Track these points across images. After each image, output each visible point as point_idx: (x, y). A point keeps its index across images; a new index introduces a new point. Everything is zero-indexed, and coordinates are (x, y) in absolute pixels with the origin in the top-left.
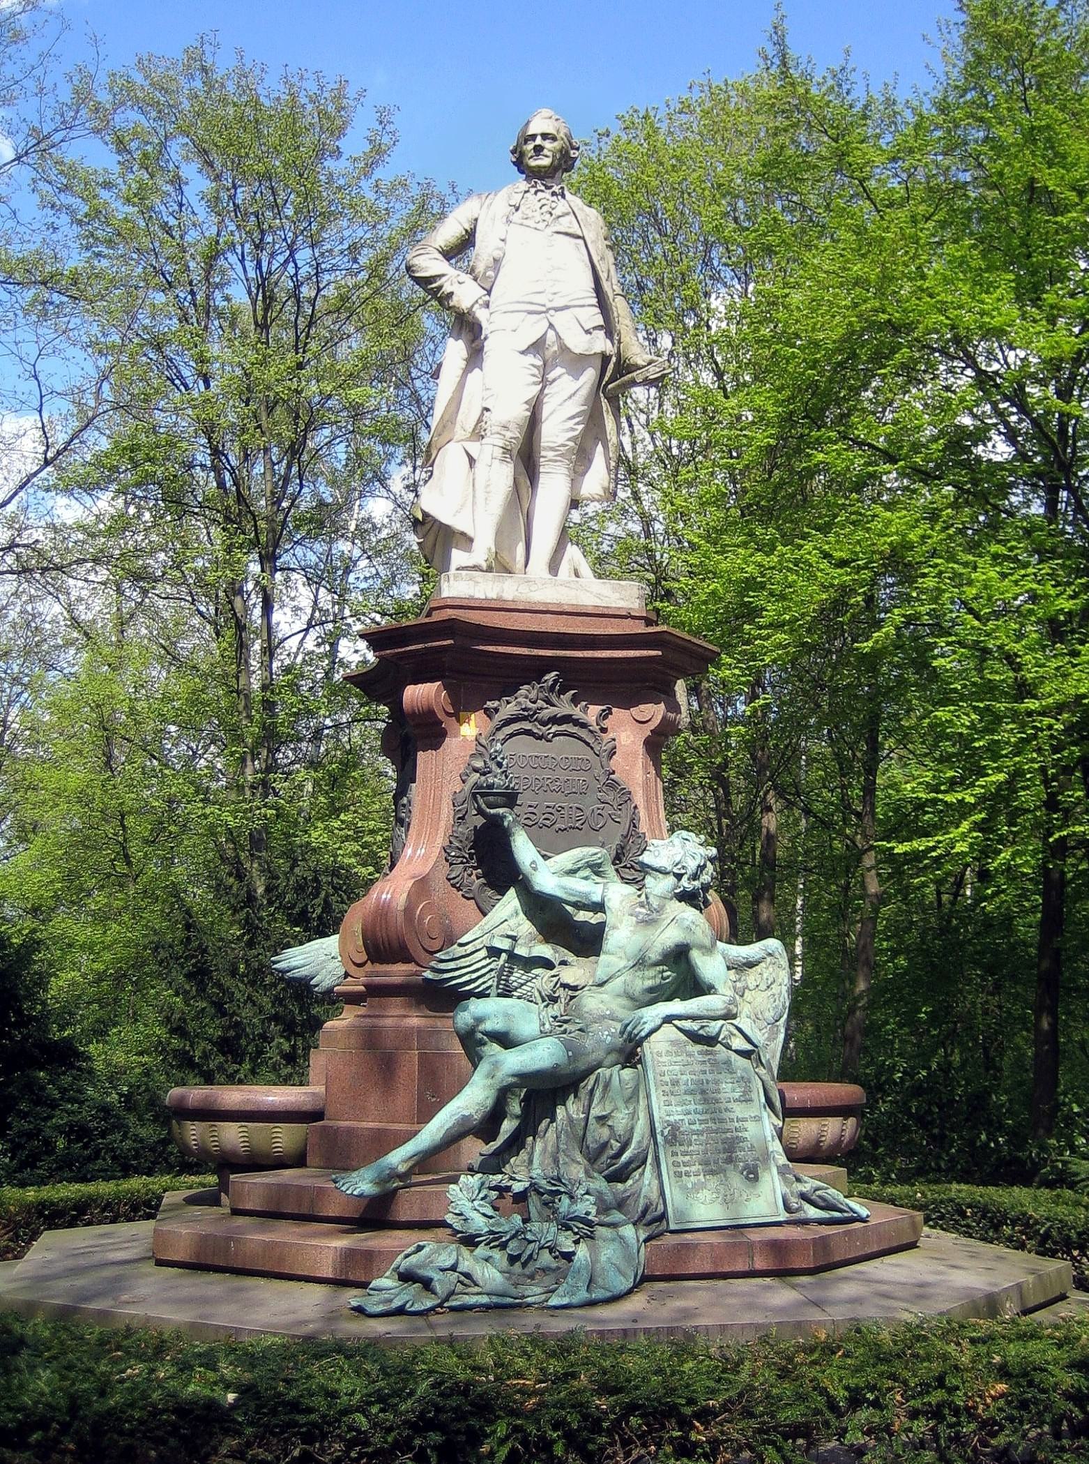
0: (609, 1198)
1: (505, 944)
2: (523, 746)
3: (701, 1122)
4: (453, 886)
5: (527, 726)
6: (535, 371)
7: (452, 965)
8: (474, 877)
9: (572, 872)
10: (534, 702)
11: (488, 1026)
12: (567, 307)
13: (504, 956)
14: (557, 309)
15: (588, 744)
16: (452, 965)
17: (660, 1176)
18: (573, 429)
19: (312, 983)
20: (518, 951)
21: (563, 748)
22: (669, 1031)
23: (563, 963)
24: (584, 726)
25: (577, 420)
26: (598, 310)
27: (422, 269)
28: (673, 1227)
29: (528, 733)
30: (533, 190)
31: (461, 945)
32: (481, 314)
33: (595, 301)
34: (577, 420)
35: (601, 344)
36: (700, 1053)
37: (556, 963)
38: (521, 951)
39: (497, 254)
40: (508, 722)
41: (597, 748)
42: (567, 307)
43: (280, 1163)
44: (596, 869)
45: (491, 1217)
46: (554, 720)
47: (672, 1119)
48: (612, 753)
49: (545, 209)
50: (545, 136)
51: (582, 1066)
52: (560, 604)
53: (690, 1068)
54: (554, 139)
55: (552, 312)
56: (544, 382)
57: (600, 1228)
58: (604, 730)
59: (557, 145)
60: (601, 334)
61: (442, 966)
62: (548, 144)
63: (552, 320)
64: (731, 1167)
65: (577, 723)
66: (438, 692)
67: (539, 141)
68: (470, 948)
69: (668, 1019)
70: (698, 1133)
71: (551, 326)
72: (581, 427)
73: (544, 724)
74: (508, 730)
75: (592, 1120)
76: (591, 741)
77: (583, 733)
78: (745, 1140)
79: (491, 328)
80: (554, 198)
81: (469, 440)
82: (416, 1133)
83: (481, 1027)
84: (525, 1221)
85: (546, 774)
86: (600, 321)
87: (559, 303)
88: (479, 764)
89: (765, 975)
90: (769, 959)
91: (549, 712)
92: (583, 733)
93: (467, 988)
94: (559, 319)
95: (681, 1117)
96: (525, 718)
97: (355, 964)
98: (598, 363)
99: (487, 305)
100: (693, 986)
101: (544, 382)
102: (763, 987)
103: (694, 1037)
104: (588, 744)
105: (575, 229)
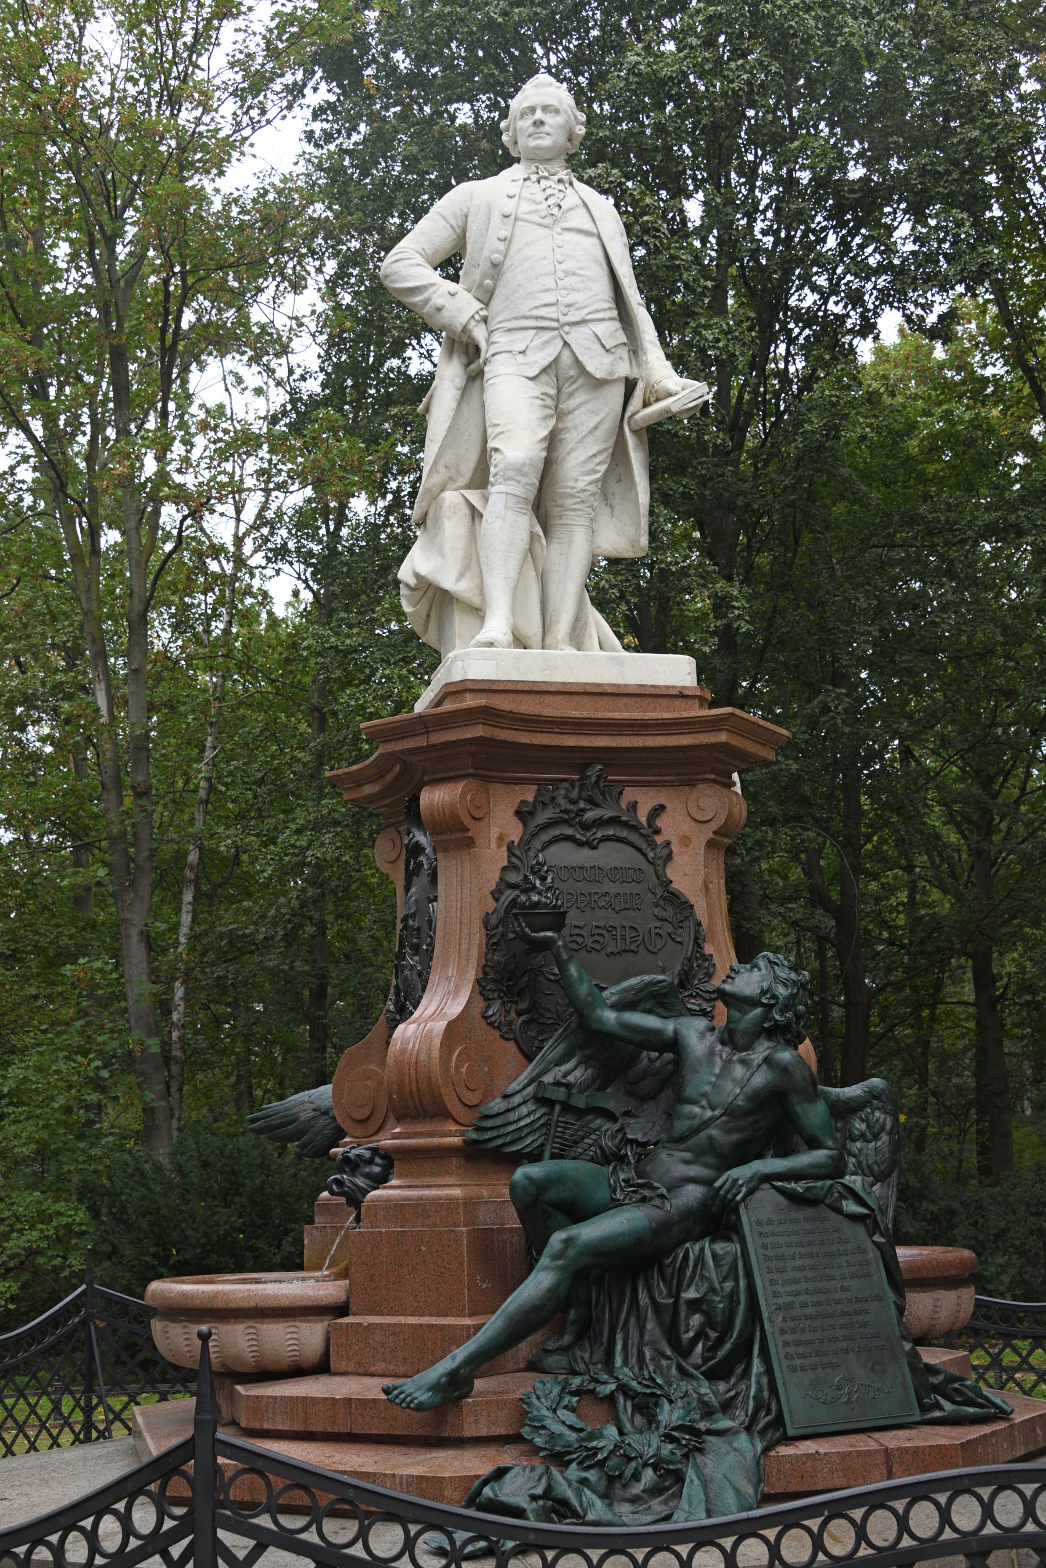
2: (564, 855)
3: (815, 1304)
4: (491, 1024)
5: (570, 832)
6: (549, 402)
7: (498, 1122)
8: (513, 1015)
10: (575, 803)
12: (582, 322)
14: (573, 324)
16: (498, 1122)
18: (595, 472)
20: (573, 1102)
21: (611, 856)
22: (767, 1195)
23: (627, 1114)
24: (635, 828)
25: (597, 460)
26: (617, 325)
27: (404, 279)
28: (791, 1432)
30: (534, 177)
31: (506, 1097)
32: (479, 333)
33: (615, 313)
34: (597, 460)
35: (624, 369)
36: (808, 1220)
39: (497, 257)
40: (544, 827)
41: (651, 855)
42: (582, 322)
43: (297, 1371)
45: (581, 1430)
46: (601, 823)
49: (551, 201)
50: (545, 108)
52: (599, 685)
53: (794, 1239)
54: (557, 112)
55: (567, 328)
56: (560, 414)
57: (709, 1438)
59: (560, 119)
60: (624, 353)
62: (548, 119)
63: (567, 338)
65: (625, 825)
66: (463, 795)
67: (539, 115)
69: (768, 1178)
70: (808, 1317)
71: (566, 344)
72: (603, 468)
74: (545, 837)
75: (683, 1308)
76: (644, 846)
77: (634, 837)
79: (493, 349)
80: (561, 187)
81: (468, 487)
82: (478, 1328)
84: (621, 1433)
86: (622, 338)
88: (514, 878)
91: (590, 815)
92: (634, 837)
93: (514, 1148)
94: (577, 338)
95: (790, 1299)
96: (565, 822)
97: (358, 1122)
98: (620, 390)
99: (485, 320)
101: (560, 414)
103: (792, 1197)
104: (639, 850)
105: (589, 226)
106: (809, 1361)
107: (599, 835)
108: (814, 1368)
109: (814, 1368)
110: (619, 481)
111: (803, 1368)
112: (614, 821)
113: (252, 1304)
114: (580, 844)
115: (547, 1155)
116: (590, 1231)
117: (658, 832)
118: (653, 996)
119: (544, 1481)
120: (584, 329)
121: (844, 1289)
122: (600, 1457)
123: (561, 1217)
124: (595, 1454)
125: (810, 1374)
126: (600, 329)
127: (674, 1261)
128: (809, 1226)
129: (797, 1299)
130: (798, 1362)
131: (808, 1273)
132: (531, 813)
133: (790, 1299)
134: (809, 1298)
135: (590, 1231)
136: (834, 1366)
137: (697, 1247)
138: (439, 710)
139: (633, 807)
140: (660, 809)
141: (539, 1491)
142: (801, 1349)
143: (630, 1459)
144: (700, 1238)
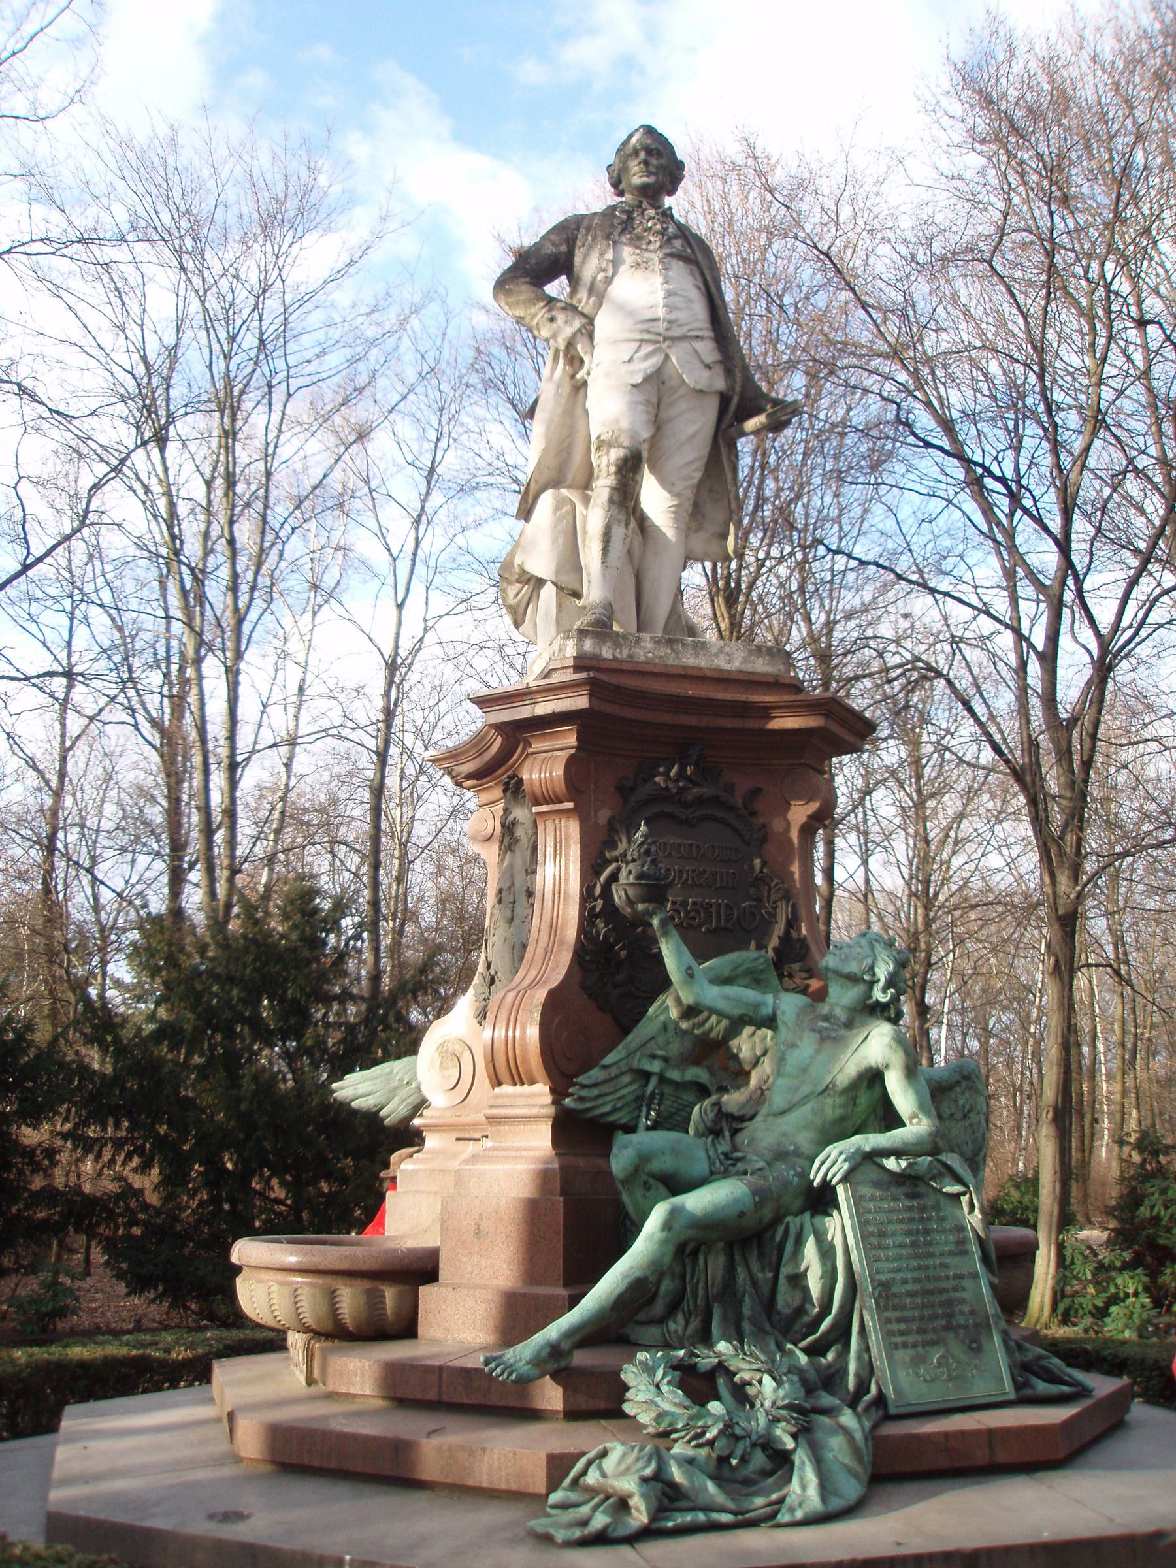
0: (812, 1375)
1: (655, 1067)
3: (917, 1281)
5: (668, 809)
9: (727, 981)
11: (656, 1166)
13: (654, 1081)
15: (736, 830)
16: (595, 1092)
17: (868, 1350)
18: (691, 478)
19: (382, 1113)
24: (732, 808)
28: (893, 1410)
29: (671, 816)
31: (605, 1067)
37: (712, 1088)
38: (674, 1075)
44: (755, 979)
46: (700, 801)
47: (883, 1277)
48: (765, 839)
51: (768, 1213)
58: (753, 814)
61: (584, 1093)
64: (950, 1335)
68: (614, 1071)
70: (912, 1294)
73: (686, 806)
75: (782, 1280)
78: (963, 1301)
83: (648, 1168)
85: (60, 887)
87: (676, 332)
89: (961, 1102)
90: (964, 1083)
95: (892, 1275)
100: (890, 1119)
102: (959, 1115)
104: (736, 830)
106: (910, 1339)
107: (698, 814)
108: (915, 1346)
109: (915, 1346)
110: (711, 490)
111: (905, 1345)
112: (714, 800)
113: (1039, 1475)
114: (686, 822)
115: (641, 1126)
116: (697, 1201)
117: (753, 814)
118: (750, 972)
119: (653, 1465)
120: (685, 345)
121: (944, 1266)
122: (708, 1436)
123: (662, 1189)
124: (703, 1434)
125: (910, 1352)
126: (700, 346)
127: (773, 1236)
128: (908, 1203)
129: (898, 1276)
130: (899, 1339)
131: (910, 1250)
132: (632, 790)
133: (892, 1275)
134: (909, 1275)
135: (697, 1201)
136: (934, 1343)
137: (798, 1219)
138: (548, 681)
139: (730, 788)
140: (758, 791)
141: (648, 1471)
142: (902, 1326)
143: (738, 1439)
144: (801, 1211)
